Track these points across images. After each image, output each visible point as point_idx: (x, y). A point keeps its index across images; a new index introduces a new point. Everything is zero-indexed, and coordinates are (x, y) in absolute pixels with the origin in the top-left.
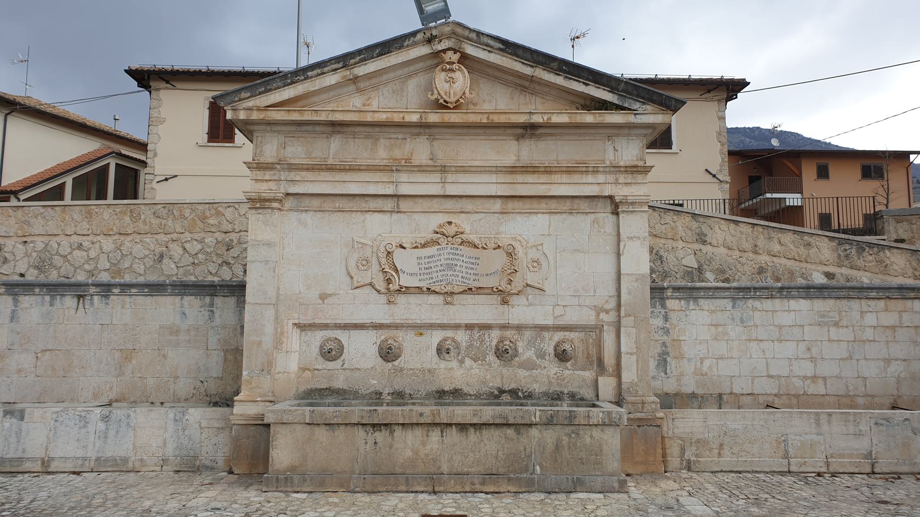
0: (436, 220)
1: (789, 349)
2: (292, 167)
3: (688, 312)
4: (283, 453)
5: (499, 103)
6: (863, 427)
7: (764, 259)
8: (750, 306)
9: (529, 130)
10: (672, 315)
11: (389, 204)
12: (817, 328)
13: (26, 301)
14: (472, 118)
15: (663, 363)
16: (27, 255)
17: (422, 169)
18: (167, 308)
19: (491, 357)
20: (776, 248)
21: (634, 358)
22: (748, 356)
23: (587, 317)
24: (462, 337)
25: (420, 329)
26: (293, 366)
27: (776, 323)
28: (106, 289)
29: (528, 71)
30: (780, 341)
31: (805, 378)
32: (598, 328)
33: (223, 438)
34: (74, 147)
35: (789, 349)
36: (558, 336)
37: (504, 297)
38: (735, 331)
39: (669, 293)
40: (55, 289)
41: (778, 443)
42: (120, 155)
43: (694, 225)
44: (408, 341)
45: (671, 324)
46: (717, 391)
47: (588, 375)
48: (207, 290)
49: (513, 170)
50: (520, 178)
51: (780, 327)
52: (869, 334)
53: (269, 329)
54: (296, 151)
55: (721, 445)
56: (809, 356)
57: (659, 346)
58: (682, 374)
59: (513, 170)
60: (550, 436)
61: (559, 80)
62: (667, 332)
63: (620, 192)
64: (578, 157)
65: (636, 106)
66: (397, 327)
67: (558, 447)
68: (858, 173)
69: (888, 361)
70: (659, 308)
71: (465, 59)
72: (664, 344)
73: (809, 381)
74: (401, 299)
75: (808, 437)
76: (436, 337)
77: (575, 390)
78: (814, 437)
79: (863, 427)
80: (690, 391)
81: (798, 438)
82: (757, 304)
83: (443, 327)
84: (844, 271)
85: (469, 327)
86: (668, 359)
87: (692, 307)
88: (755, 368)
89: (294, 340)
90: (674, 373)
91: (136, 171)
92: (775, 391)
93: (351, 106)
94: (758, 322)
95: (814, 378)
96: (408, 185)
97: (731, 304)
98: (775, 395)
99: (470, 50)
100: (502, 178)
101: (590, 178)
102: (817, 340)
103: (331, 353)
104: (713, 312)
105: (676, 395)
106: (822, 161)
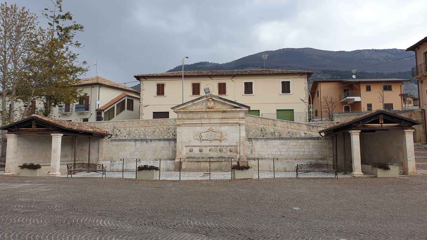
0: (209, 127)
1: (275, 150)
2: (184, 119)
4: (184, 166)
5: (219, 107)
6: (284, 163)
7: (290, 130)
9: (224, 112)
11: (200, 125)
13: (137, 142)
14: (214, 110)
15: (251, 152)
16: (126, 132)
17: (206, 119)
18: (162, 143)
19: (218, 151)
20: (293, 127)
23: (235, 144)
24: (213, 148)
25: (206, 146)
26: (185, 153)
28: (151, 140)
29: (223, 102)
32: (237, 146)
33: (174, 165)
34: (114, 95)
35: (275, 150)
36: (230, 147)
37: (220, 141)
38: (265, 146)
40: (142, 140)
42: (128, 96)
43: (273, 122)
44: (204, 149)
47: (235, 154)
48: (169, 140)
49: (221, 118)
50: (223, 120)
52: (291, 147)
53: (181, 147)
54: (184, 116)
59: (221, 118)
60: (225, 163)
61: (229, 103)
63: (240, 122)
65: (242, 107)
66: (202, 146)
67: (227, 165)
68: (382, 88)
69: (294, 152)
71: (213, 100)
74: (203, 141)
76: (209, 148)
79: (284, 163)
83: (210, 146)
84: (309, 132)
85: (214, 146)
89: (185, 149)
91: (133, 100)
93: (193, 108)
96: (204, 121)
99: (213, 98)
100: (220, 120)
101: (235, 120)
103: (191, 151)
106: (368, 85)
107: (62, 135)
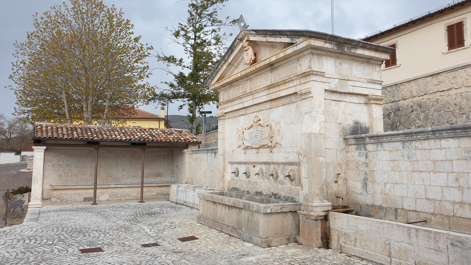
1: (441, 179)
3: (377, 152)
6: (442, 245)
8: (414, 146)
10: (370, 155)
12: (464, 162)
15: (365, 185)
21: (307, 180)
22: (413, 183)
27: (432, 159)
30: (435, 172)
31: (454, 203)
35: (441, 179)
38: (404, 165)
39: (368, 140)
41: (386, 245)
45: (369, 160)
46: (394, 206)
50: (271, 91)
51: (435, 161)
55: (356, 239)
56: (457, 185)
57: (363, 174)
58: (374, 193)
62: (367, 165)
64: (288, 75)
70: (363, 151)
72: (366, 173)
73: (457, 206)
75: (404, 245)
77: (294, 196)
78: (407, 245)
80: (379, 204)
81: (396, 243)
82: (418, 144)
86: (368, 183)
87: (379, 149)
88: (417, 192)
90: (371, 192)
92: (432, 211)
94: (419, 158)
95: (462, 203)
97: (402, 145)
98: (432, 214)
102: (463, 172)
104: (391, 151)
105: (372, 206)
107: (45, 148)
